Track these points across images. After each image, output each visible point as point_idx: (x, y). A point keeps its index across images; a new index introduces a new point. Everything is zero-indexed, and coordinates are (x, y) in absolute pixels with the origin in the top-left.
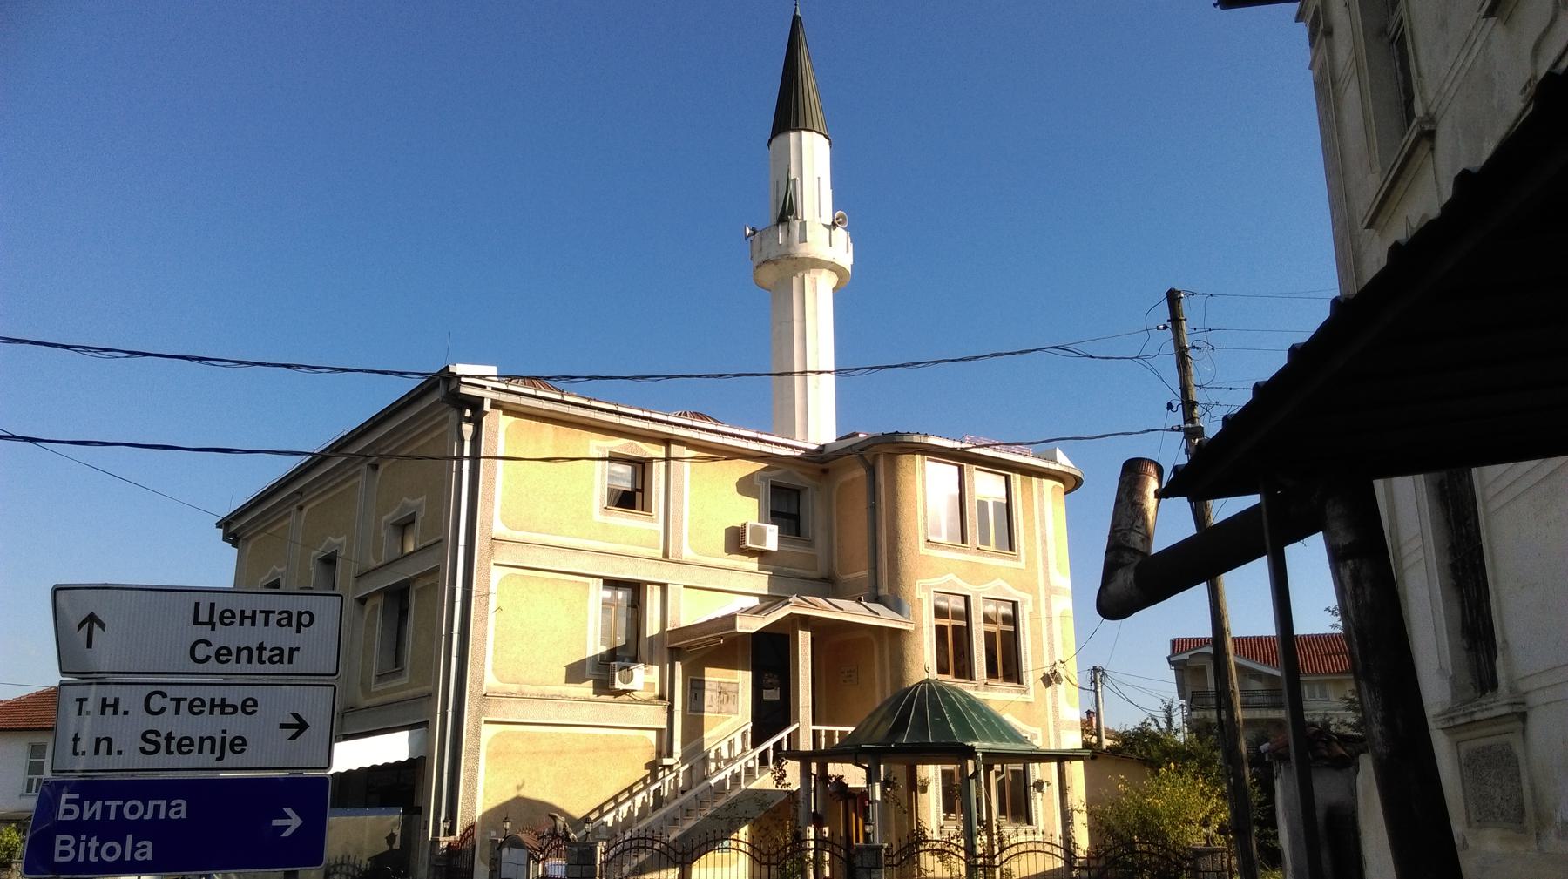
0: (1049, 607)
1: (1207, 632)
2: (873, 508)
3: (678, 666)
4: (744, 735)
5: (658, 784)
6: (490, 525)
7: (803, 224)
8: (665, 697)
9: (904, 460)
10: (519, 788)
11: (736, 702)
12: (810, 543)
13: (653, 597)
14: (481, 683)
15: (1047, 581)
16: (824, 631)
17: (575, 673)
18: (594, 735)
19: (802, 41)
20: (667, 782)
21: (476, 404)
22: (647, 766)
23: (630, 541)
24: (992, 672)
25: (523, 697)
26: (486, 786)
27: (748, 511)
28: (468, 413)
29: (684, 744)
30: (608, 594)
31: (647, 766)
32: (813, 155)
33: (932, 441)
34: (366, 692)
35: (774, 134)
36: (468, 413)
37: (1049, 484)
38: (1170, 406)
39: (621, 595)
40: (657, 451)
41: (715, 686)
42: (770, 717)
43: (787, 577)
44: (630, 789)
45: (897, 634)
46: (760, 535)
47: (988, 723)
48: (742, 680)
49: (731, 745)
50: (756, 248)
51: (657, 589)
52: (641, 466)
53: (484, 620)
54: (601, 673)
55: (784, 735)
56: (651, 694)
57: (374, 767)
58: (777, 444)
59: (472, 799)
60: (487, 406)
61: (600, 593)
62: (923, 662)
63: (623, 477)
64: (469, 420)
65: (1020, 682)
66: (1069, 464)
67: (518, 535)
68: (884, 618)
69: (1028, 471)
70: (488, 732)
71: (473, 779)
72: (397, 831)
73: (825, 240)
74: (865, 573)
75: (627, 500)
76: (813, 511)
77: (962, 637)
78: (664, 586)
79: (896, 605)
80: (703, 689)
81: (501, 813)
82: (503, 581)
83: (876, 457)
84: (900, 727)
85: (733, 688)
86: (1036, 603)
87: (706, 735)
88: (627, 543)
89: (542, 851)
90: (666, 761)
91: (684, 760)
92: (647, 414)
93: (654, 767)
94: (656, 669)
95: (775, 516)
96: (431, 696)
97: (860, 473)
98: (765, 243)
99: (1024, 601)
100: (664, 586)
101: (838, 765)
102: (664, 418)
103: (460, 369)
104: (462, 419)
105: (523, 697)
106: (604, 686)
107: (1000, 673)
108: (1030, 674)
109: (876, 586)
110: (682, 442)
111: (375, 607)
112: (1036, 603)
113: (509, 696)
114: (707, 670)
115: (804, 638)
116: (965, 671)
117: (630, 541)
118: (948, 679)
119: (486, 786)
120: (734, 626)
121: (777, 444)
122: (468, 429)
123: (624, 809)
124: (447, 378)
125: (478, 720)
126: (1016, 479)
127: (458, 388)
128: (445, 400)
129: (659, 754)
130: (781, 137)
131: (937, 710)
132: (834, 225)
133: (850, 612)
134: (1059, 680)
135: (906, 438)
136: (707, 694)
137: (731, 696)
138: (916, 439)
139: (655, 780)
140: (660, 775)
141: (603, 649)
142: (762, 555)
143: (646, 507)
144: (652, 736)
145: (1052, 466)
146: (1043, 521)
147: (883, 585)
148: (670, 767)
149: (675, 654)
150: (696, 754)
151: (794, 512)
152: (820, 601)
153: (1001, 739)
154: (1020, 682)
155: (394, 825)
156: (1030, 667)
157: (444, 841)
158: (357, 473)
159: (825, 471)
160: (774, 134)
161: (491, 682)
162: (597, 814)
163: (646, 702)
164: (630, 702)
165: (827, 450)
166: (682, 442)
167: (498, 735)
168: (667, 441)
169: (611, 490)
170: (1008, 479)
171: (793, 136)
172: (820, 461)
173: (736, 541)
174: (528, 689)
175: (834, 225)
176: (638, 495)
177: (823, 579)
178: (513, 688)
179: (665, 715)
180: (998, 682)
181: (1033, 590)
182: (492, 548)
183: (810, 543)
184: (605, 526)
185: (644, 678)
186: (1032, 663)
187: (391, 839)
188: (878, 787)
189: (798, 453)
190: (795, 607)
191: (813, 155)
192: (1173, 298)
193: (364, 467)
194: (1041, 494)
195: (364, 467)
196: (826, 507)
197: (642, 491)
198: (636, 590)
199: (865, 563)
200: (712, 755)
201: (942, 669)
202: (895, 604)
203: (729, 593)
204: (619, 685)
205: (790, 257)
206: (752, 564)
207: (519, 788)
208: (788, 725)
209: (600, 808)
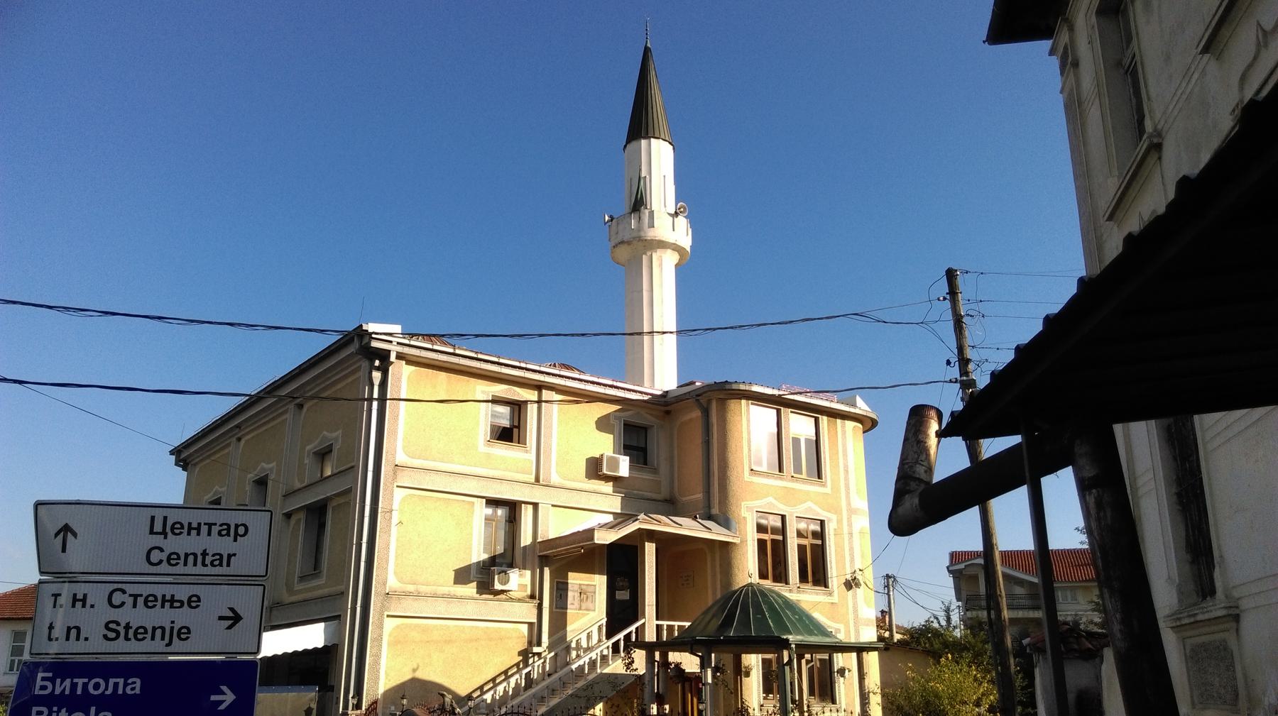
0: (850, 525)
2: (707, 443)
3: (547, 571)
4: (600, 628)
6: (394, 455)
7: (652, 213)
8: (536, 596)
9: (733, 404)
10: (414, 670)
11: (593, 601)
12: (655, 471)
14: (385, 584)
15: (849, 504)
17: (462, 576)
18: (477, 628)
20: (536, 667)
21: (384, 356)
22: (520, 653)
24: (803, 578)
25: (418, 595)
27: (604, 445)
28: (377, 363)
30: (489, 511)
31: (520, 653)
32: (659, 158)
33: (756, 388)
34: (291, 591)
35: (629, 141)
36: (377, 363)
37: (850, 425)
38: (948, 363)
40: (531, 395)
41: (576, 588)
42: (621, 613)
43: (636, 498)
44: (505, 672)
45: (726, 546)
46: (614, 464)
47: (800, 620)
48: (599, 582)
49: (589, 637)
51: (530, 508)
52: (518, 407)
54: (484, 576)
55: (633, 628)
60: (393, 357)
61: (483, 511)
62: (747, 569)
64: (378, 369)
67: (417, 463)
68: (716, 533)
69: (834, 414)
70: (389, 624)
72: (314, 706)
73: (669, 226)
74: (700, 496)
75: (506, 435)
76: (658, 446)
77: (779, 549)
78: (535, 505)
79: (725, 522)
81: (400, 691)
82: (404, 500)
83: (709, 402)
84: (727, 623)
85: (591, 589)
86: (840, 522)
87: (569, 628)
88: (506, 470)
90: (536, 650)
91: (550, 648)
92: (523, 365)
93: (525, 654)
94: (528, 573)
95: (627, 449)
96: (343, 594)
97: (696, 414)
98: (621, 227)
99: (830, 520)
100: (535, 505)
101: (677, 654)
102: (537, 368)
103: (371, 327)
104: (373, 368)
105: (418, 595)
106: (486, 587)
107: (810, 579)
108: (835, 580)
110: (551, 388)
112: (840, 522)
113: (408, 594)
114: (570, 574)
115: (650, 549)
116: (781, 577)
118: (768, 584)
120: (593, 539)
122: (377, 376)
123: (500, 689)
124: (361, 335)
126: (824, 420)
129: (530, 643)
131: (759, 610)
132: (676, 214)
134: (858, 585)
135: (734, 387)
136: (570, 594)
137: (590, 595)
138: (742, 387)
139: (526, 665)
140: (531, 661)
141: (485, 556)
142: (616, 480)
143: (521, 441)
144: (525, 628)
145: (852, 410)
146: (845, 454)
147: (715, 506)
148: (539, 654)
149: (544, 561)
152: (663, 518)
153: (811, 633)
154: (826, 586)
156: (835, 574)
160: (629, 141)
161: (393, 583)
162: (478, 693)
163: (519, 600)
165: (670, 395)
166: (551, 388)
167: (398, 627)
168: (539, 387)
169: (493, 427)
170: (817, 420)
171: (644, 142)
172: (664, 404)
173: (595, 468)
174: (423, 589)
175: (676, 214)
176: (516, 431)
177: (666, 501)
178: (411, 588)
179: (535, 611)
180: (808, 586)
181: (837, 511)
183: (655, 471)
184: (488, 456)
185: (519, 580)
188: (709, 672)
189: (646, 398)
190: (643, 523)
191: (659, 158)
192: (951, 275)
194: (844, 433)
196: (669, 442)
197: (518, 427)
198: (513, 508)
200: (573, 645)
201: (763, 575)
203: (589, 511)
204: (498, 586)
205: (640, 239)
206: (608, 487)
207: (414, 670)
208: (636, 620)
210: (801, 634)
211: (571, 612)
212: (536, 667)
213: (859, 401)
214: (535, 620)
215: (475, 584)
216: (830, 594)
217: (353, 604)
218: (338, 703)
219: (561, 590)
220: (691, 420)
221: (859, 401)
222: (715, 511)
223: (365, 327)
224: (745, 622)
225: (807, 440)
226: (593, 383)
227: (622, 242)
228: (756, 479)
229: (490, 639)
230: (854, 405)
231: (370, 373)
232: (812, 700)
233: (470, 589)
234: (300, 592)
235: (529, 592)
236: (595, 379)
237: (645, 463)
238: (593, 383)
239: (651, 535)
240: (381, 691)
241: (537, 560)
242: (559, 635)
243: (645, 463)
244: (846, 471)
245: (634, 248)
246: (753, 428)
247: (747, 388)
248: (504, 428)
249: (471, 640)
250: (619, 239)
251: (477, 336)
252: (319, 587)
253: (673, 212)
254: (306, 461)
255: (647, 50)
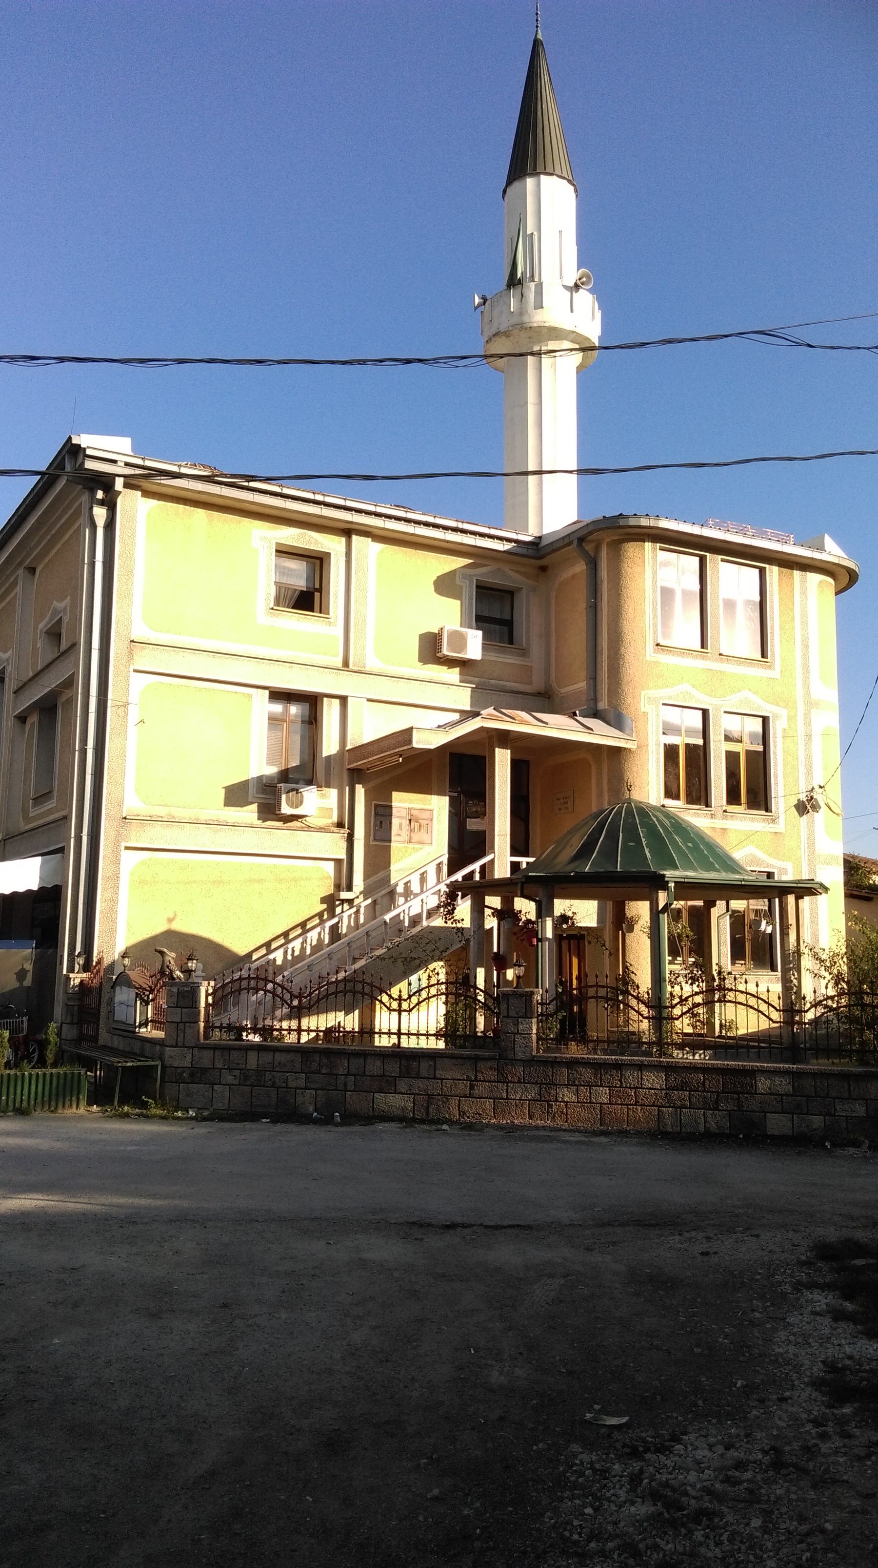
0: (808, 724)
1: (544, 469)
2: (594, 609)
3: (360, 791)
4: (439, 867)
5: (335, 920)
7: (540, 286)
8: (345, 824)
9: (631, 549)
10: (170, 920)
11: (429, 830)
12: (524, 652)
13: (330, 712)
14: (121, 804)
15: (808, 694)
16: (531, 756)
17: (236, 795)
19: (543, 63)
20: (345, 918)
21: (105, 482)
22: (323, 900)
23: (303, 649)
24: (733, 797)
25: (171, 821)
26: (128, 915)
27: (448, 615)
28: (100, 495)
29: (366, 876)
30: (278, 708)
31: (323, 900)
32: (553, 204)
33: (664, 524)
34: (27, 818)
35: (509, 182)
36: (100, 495)
37: (813, 578)
39: (294, 709)
40: (332, 544)
41: (404, 813)
42: (467, 844)
43: (487, 686)
44: (303, 925)
45: (616, 752)
46: (459, 640)
47: (696, 849)
48: (438, 806)
49: (423, 879)
50: (486, 320)
51: (336, 703)
52: (318, 562)
53: (124, 734)
54: (267, 797)
55: (476, 866)
56: (328, 821)
57: (15, 894)
58: (482, 535)
59: (112, 933)
60: (119, 483)
61: (266, 707)
62: (648, 785)
63: (298, 576)
64: (102, 503)
65: (768, 809)
66: (841, 553)
68: (600, 734)
69: (788, 563)
70: (129, 859)
71: (112, 909)
72: (29, 966)
73: (566, 306)
74: (582, 685)
75: (307, 600)
76: (529, 617)
77: (698, 757)
78: (343, 700)
79: (616, 720)
80: (390, 815)
81: (151, 948)
83: (597, 549)
84: (584, 852)
85: (426, 815)
87: (393, 867)
89: (151, 991)
90: (344, 895)
91: (366, 893)
92: (319, 498)
93: (331, 902)
94: (333, 793)
95: (481, 621)
96: (66, 818)
97: (580, 567)
98: (496, 313)
99: (776, 716)
100: (343, 700)
101: (568, 902)
102: (341, 502)
103: (84, 440)
104: (94, 501)
105: (171, 821)
106: (269, 811)
107: (743, 798)
108: (781, 801)
109: (595, 700)
110: (366, 532)
111: (33, 725)
112: (791, 719)
113: (152, 820)
114: (395, 795)
115: (503, 759)
116: (699, 795)
117: (303, 649)
118: (677, 806)
119: (128, 915)
121: (482, 535)
122: (100, 514)
123: (297, 945)
124: (73, 451)
125: (117, 847)
126: (773, 572)
127: (83, 463)
128: (71, 486)
129: (338, 887)
130: (516, 185)
131: (632, 834)
132: (577, 287)
133: (558, 727)
134: (816, 807)
135: (632, 522)
136: (395, 822)
137: (424, 823)
138: (644, 522)
139: (332, 915)
140: (338, 910)
141: (272, 770)
142: (464, 665)
143: (323, 609)
144: (330, 867)
145: (817, 555)
146: (805, 623)
147: (602, 698)
148: (350, 902)
149: (356, 775)
150: (382, 891)
151: (507, 617)
152: (524, 715)
153: (710, 868)
154: (768, 809)
155: (25, 959)
156: (781, 792)
157: (76, 978)
158: (15, 584)
159: (543, 569)
160: (509, 182)
161: (132, 805)
162: (263, 951)
163: (320, 829)
164: (301, 829)
165: (544, 543)
166: (366, 532)
168: (347, 532)
169: (279, 586)
170: (762, 573)
171: (530, 182)
172: (538, 555)
173: (431, 649)
174: (179, 814)
175: (577, 287)
176: (317, 595)
177: (539, 694)
178: (162, 812)
179: (344, 845)
180: (741, 809)
182: (131, 652)
183: (524, 652)
185: (318, 802)
186: (784, 788)
187: (21, 975)
188: (549, 923)
189: (507, 546)
190: (492, 720)
191: (553, 204)
193: (21, 571)
194: (804, 592)
195: (21, 571)
196: (538, 607)
197: (320, 590)
198: (312, 702)
199: (583, 674)
200: (400, 889)
201: (671, 792)
202: (615, 719)
203: (438, 711)
204: (286, 809)
205: (522, 327)
206: (453, 675)
207: (170, 920)
209: (268, 944)
210: (695, 870)
211: (396, 846)
212: (345, 918)
213: (829, 543)
214: (343, 855)
215: (254, 807)
216: (773, 821)
217: (77, 834)
218: (61, 963)
219: (381, 817)
220: (573, 576)
221: (829, 543)
222: (603, 705)
223: (75, 441)
224: (610, 852)
225: (748, 602)
226: (427, 524)
227: (497, 334)
228: (664, 658)
229: (279, 880)
230: (821, 548)
231: (91, 509)
232: (739, 968)
233: (250, 813)
234: (35, 818)
235: (335, 819)
236: (431, 519)
237: (511, 642)
238: (427, 524)
239: (504, 738)
240: (120, 947)
241: (346, 776)
242: (381, 875)
243: (511, 642)
244: (806, 647)
245: (517, 347)
246: (657, 576)
247: (652, 523)
248: (302, 591)
249: (252, 881)
250: (494, 331)
251: (62, 360)
252: (50, 812)
253: (572, 284)
254: (39, 645)
255: (537, 43)
